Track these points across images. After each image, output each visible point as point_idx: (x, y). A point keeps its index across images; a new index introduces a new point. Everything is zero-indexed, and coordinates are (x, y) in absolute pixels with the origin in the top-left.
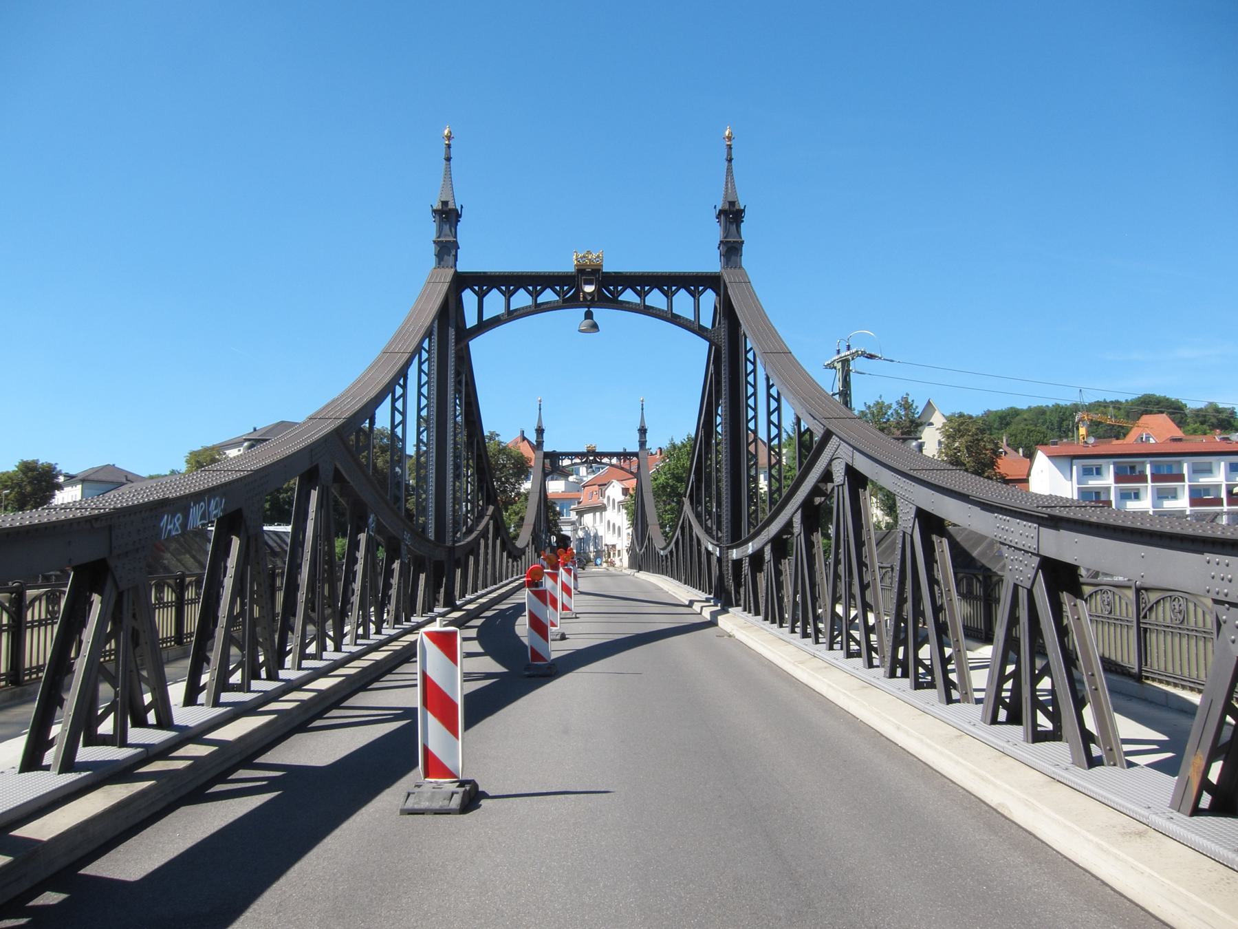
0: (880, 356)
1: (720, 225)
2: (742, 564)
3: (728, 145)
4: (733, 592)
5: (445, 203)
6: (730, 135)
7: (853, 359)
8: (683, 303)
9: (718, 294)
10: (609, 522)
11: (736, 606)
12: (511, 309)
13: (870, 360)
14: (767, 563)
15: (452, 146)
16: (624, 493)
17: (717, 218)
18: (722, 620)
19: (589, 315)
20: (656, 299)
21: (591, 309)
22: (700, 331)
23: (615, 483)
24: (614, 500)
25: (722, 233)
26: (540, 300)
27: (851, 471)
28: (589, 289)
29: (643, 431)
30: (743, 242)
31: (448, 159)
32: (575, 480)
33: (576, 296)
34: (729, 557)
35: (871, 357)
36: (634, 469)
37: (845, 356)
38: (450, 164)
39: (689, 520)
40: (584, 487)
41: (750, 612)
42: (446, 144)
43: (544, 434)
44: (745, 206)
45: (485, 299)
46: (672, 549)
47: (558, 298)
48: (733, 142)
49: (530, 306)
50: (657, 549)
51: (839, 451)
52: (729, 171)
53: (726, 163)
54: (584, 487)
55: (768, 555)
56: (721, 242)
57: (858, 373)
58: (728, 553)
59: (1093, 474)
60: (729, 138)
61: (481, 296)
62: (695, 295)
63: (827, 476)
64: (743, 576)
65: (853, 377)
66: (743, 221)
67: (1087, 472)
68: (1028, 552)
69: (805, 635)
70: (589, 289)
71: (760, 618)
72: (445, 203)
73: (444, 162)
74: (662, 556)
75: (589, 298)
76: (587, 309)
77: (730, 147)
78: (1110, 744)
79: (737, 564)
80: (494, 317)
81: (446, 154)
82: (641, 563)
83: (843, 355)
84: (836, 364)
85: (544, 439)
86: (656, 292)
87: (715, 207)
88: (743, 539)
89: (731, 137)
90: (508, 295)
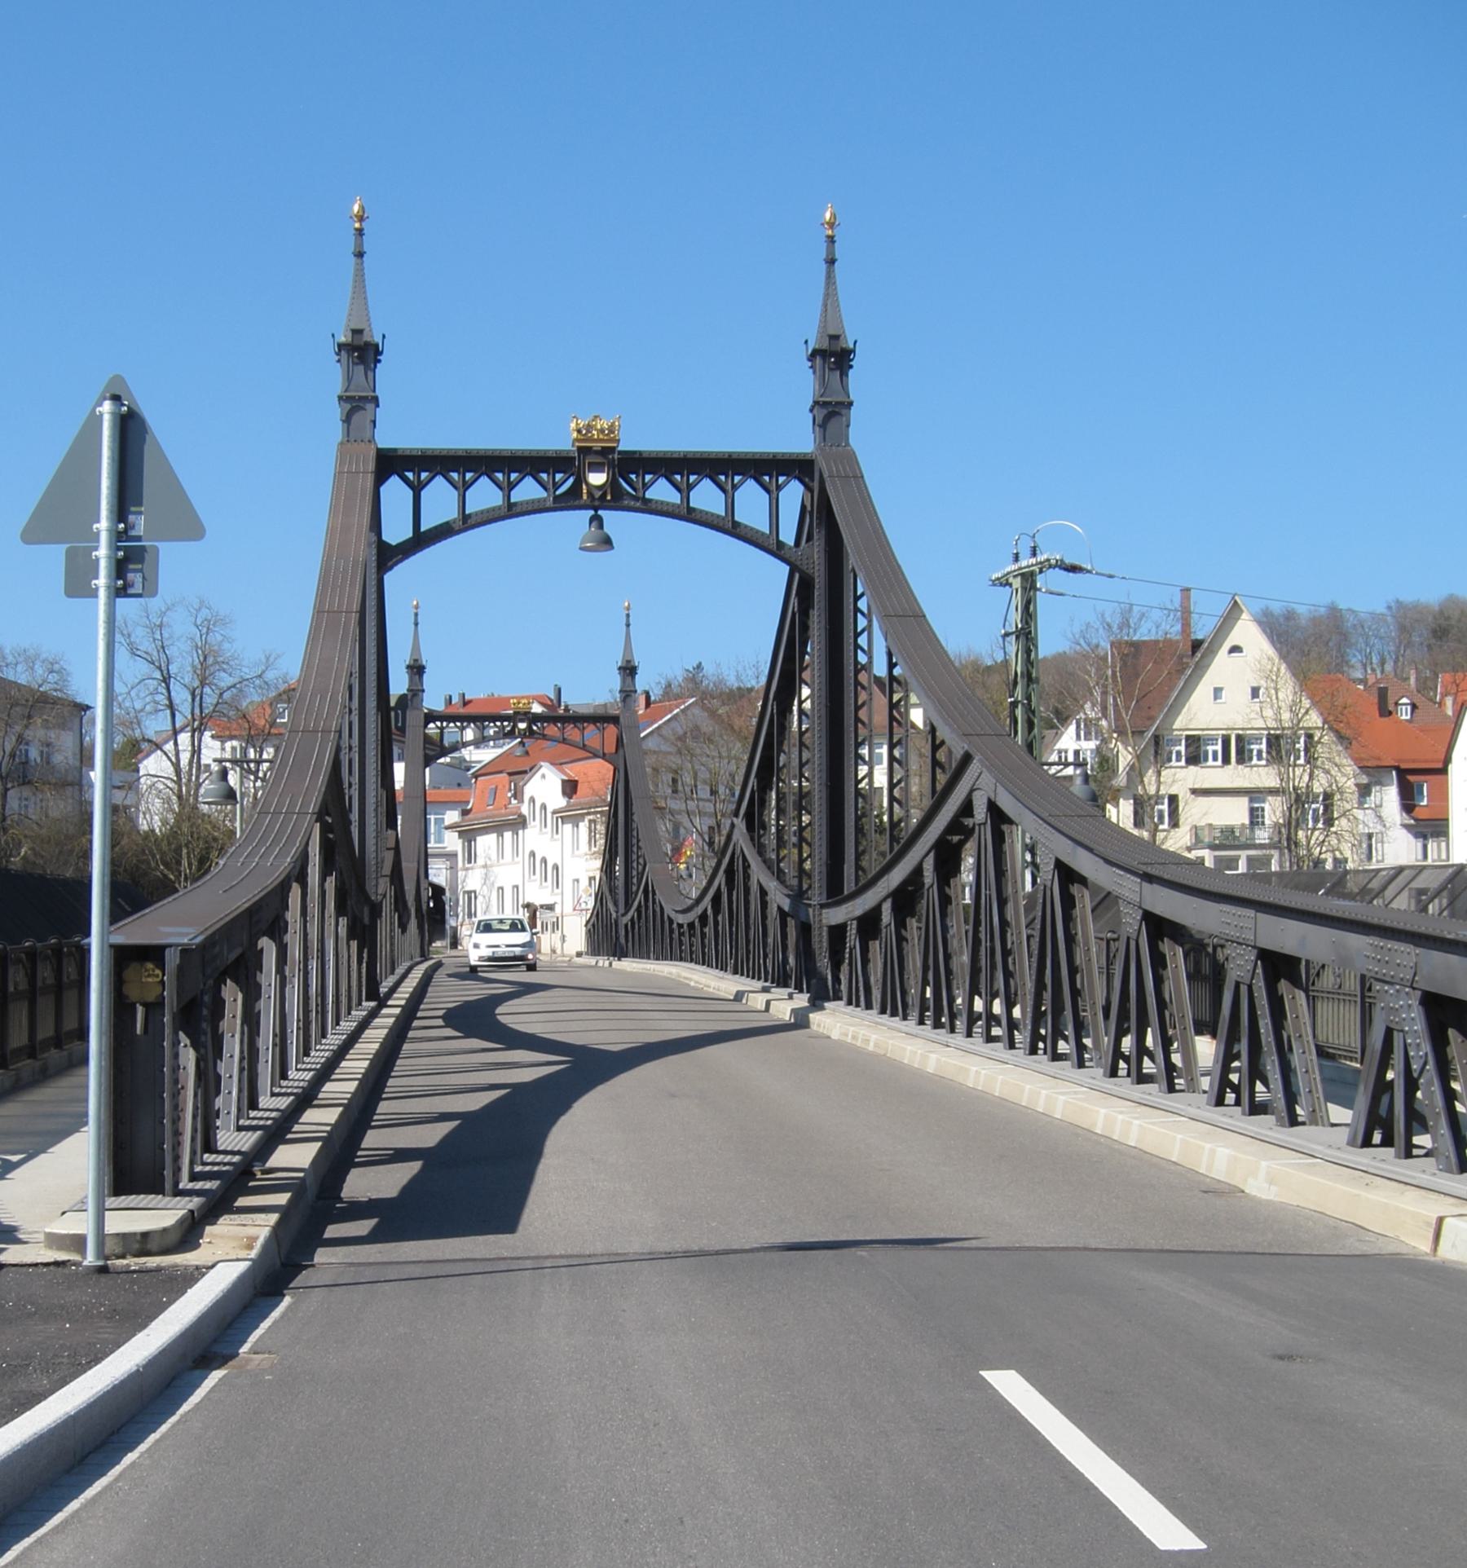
0: (1089, 568)
1: (814, 372)
2: (846, 932)
3: (828, 237)
4: (829, 977)
5: (357, 332)
7: (1041, 572)
8: (751, 503)
9: (808, 488)
10: (533, 854)
11: (834, 1000)
12: (423, 529)
13: (1071, 574)
14: (886, 927)
15: (365, 231)
16: (568, 791)
17: (809, 360)
18: (815, 1017)
19: (597, 520)
20: (706, 496)
21: (600, 512)
22: (776, 550)
23: (546, 769)
24: (544, 807)
25: (817, 387)
26: (517, 495)
27: (993, 808)
28: (597, 479)
29: (629, 670)
30: (851, 404)
31: (360, 255)
33: (575, 491)
34: (824, 921)
35: (1074, 569)
36: (610, 748)
37: (1028, 567)
38: (362, 263)
39: (744, 856)
40: (476, 776)
41: (858, 1005)
42: (356, 229)
43: (425, 676)
44: (855, 342)
45: (423, 493)
46: (706, 910)
48: (839, 234)
49: (499, 508)
50: (668, 911)
51: (980, 780)
53: (824, 266)
54: (476, 776)
55: (887, 916)
56: (816, 403)
57: (1052, 593)
58: (821, 914)
60: (831, 225)
61: (417, 489)
62: (773, 492)
63: (967, 808)
64: (848, 950)
65: (1042, 600)
66: (851, 367)
68: (1130, 903)
69: (937, 1025)
70: (597, 479)
71: (874, 1012)
72: (357, 332)
73: (353, 259)
74: (680, 926)
75: (598, 494)
78: (1192, 1074)
79: (837, 933)
80: (441, 525)
82: (623, 941)
83: (1024, 563)
84: (1011, 580)
86: (707, 483)
88: (846, 893)
89: (834, 223)
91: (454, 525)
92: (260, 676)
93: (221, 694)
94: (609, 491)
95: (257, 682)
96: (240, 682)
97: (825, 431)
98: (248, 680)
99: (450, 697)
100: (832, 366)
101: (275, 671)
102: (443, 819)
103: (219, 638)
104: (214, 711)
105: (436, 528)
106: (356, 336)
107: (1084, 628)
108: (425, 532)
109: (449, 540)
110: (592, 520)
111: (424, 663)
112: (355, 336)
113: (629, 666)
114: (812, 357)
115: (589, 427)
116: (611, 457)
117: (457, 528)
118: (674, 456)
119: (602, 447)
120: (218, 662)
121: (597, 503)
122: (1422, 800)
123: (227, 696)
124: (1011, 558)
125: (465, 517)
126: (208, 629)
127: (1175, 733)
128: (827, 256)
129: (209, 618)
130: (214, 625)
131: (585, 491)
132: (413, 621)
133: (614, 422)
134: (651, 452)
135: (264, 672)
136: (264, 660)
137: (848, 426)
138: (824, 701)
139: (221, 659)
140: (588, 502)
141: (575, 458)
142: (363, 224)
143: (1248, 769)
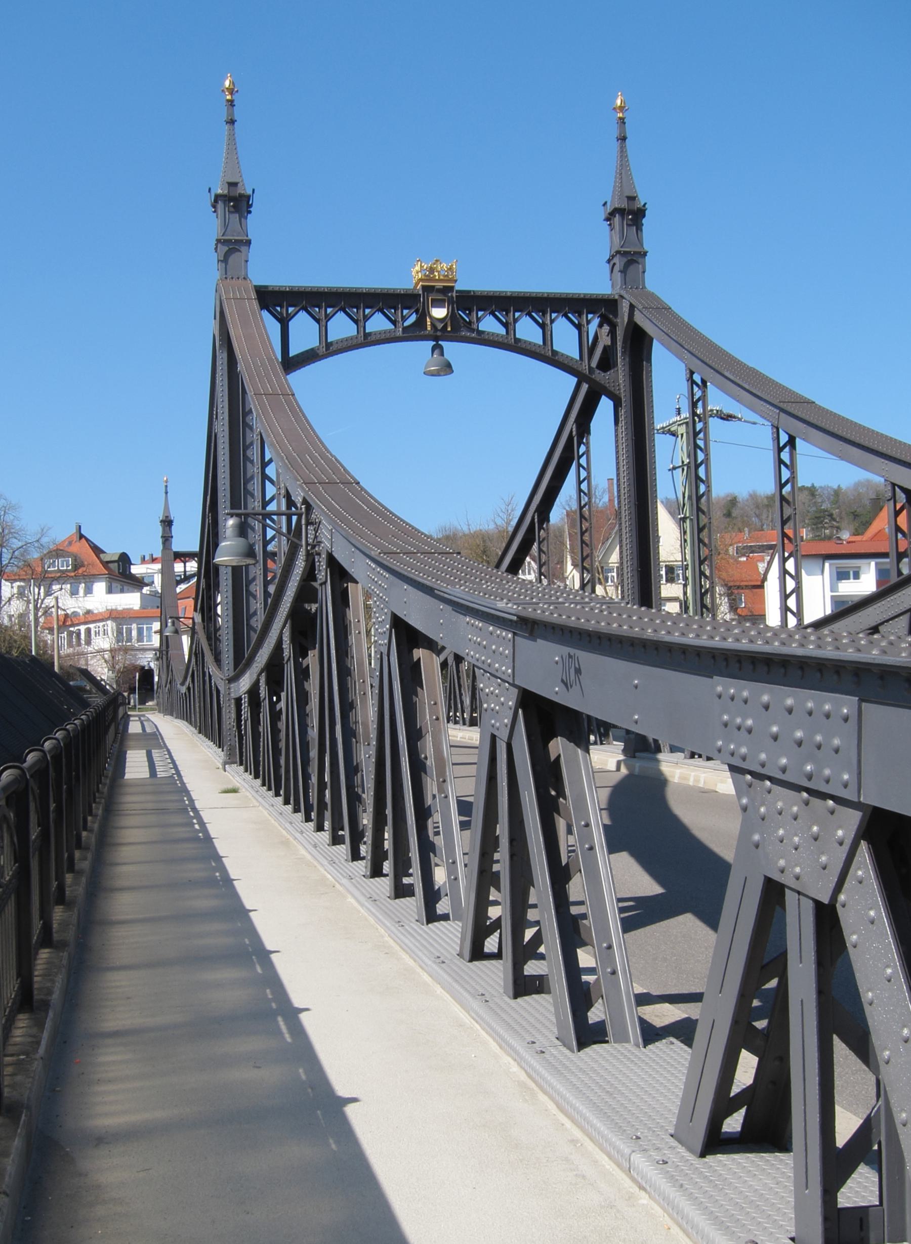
0: (740, 416)
3: (620, 118)
6: (231, 87)
15: (235, 103)
19: (437, 348)
21: (440, 342)
28: (439, 313)
30: (645, 254)
32: (148, 593)
33: (420, 323)
42: (228, 101)
43: (173, 527)
44: (254, 190)
47: (392, 327)
52: (623, 151)
56: (218, 241)
59: (849, 579)
60: (622, 108)
61: (284, 322)
67: (842, 575)
70: (439, 313)
73: (227, 127)
75: (440, 326)
76: (435, 343)
77: (622, 121)
80: (307, 351)
81: (228, 115)
85: (173, 534)
87: (210, 190)
89: (233, 89)
90: (322, 322)
91: (318, 351)
92: (38, 541)
93: (14, 552)
94: (449, 324)
95: (36, 545)
96: (25, 545)
97: (625, 276)
98: (30, 543)
99: (144, 556)
100: (630, 222)
101: (47, 538)
102: (151, 627)
103: (12, 518)
104: (9, 563)
105: (302, 354)
106: (232, 188)
107: (568, 498)
108: (293, 357)
109: (312, 366)
110: (433, 349)
111: (172, 518)
112: (231, 188)
113: (167, 520)
114: (609, 218)
115: (432, 270)
116: (450, 295)
117: (321, 354)
118: (502, 295)
119: (444, 286)
120: (11, 533)
121: (439, 334)
122: (742, 604)
123: (16, 553)
124: (674, 412)
125: (328, 345)
126: (5, 512)
127: (610, 565)
128: (620, 134)
129: (5, 505)
130: (8, 509)
131: (429, 323)
132: (164, 491)
133: (452, 265)
134: (482, 292)
135: (40, 538)
136: (40, 531)
137: (644, 272)
138: (633, 500)
139: (13, 531)
140: (432, 333)
141: (420, 295)
142: (234, 97)
143: (677, 585)
